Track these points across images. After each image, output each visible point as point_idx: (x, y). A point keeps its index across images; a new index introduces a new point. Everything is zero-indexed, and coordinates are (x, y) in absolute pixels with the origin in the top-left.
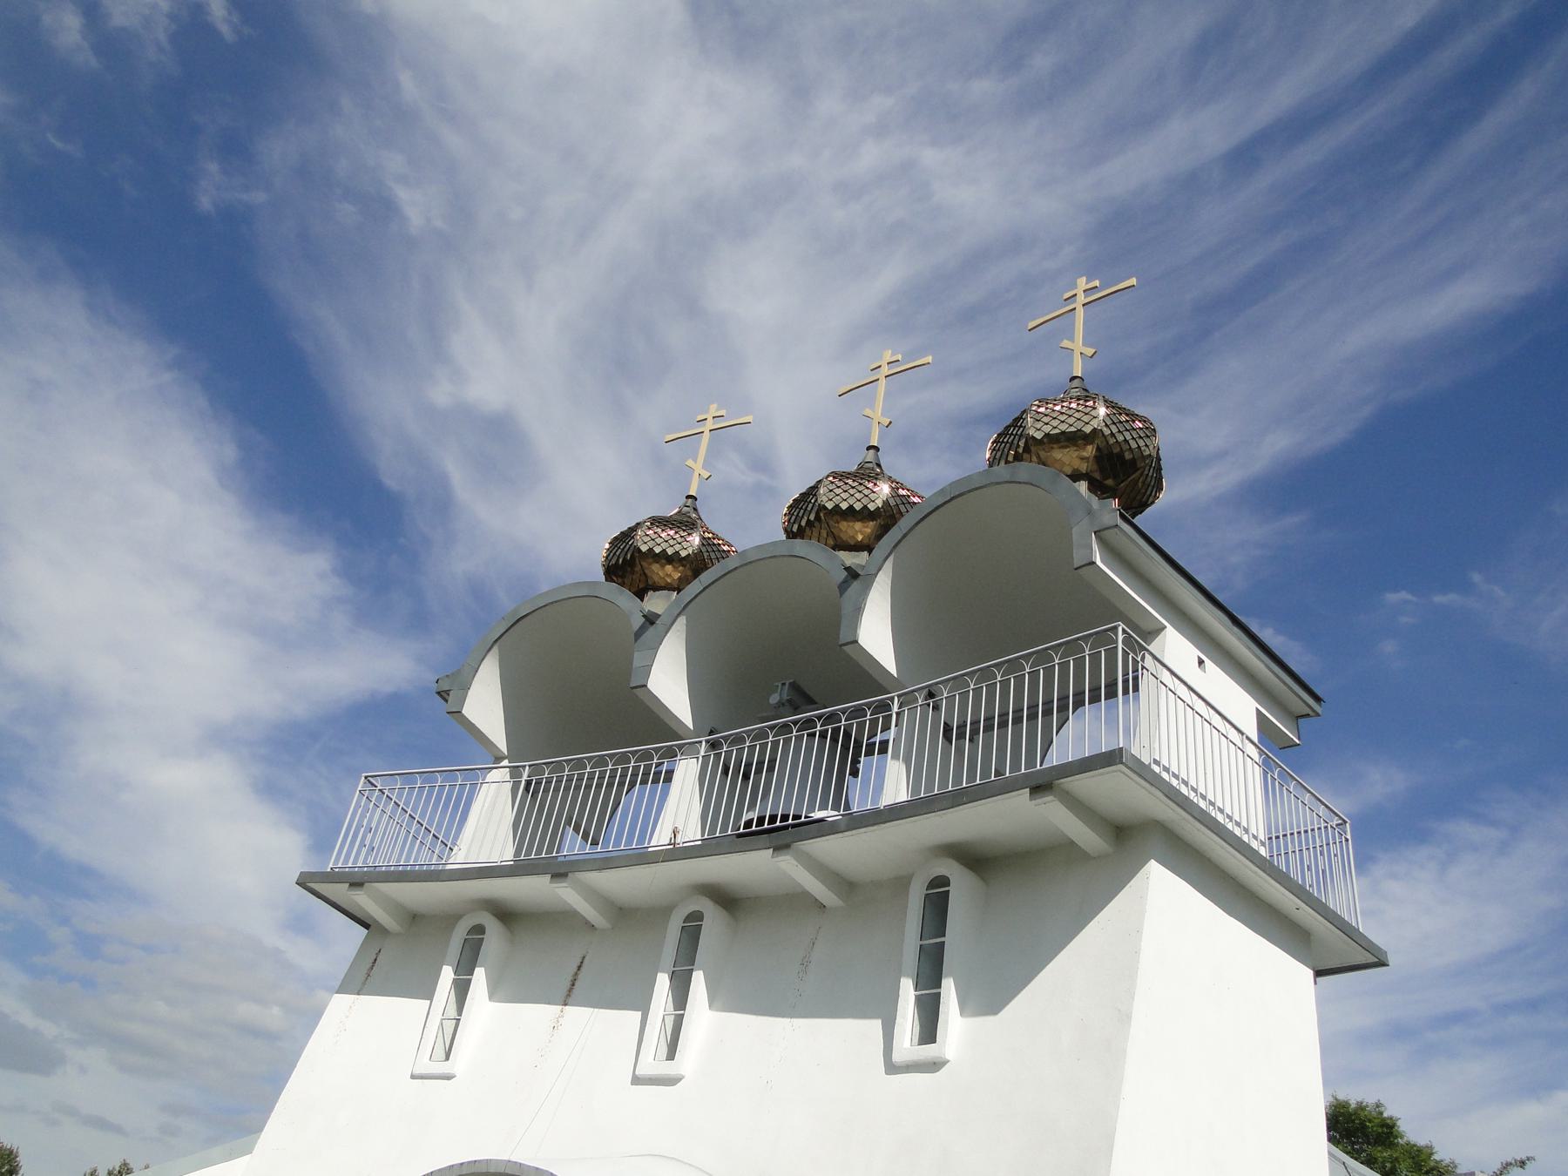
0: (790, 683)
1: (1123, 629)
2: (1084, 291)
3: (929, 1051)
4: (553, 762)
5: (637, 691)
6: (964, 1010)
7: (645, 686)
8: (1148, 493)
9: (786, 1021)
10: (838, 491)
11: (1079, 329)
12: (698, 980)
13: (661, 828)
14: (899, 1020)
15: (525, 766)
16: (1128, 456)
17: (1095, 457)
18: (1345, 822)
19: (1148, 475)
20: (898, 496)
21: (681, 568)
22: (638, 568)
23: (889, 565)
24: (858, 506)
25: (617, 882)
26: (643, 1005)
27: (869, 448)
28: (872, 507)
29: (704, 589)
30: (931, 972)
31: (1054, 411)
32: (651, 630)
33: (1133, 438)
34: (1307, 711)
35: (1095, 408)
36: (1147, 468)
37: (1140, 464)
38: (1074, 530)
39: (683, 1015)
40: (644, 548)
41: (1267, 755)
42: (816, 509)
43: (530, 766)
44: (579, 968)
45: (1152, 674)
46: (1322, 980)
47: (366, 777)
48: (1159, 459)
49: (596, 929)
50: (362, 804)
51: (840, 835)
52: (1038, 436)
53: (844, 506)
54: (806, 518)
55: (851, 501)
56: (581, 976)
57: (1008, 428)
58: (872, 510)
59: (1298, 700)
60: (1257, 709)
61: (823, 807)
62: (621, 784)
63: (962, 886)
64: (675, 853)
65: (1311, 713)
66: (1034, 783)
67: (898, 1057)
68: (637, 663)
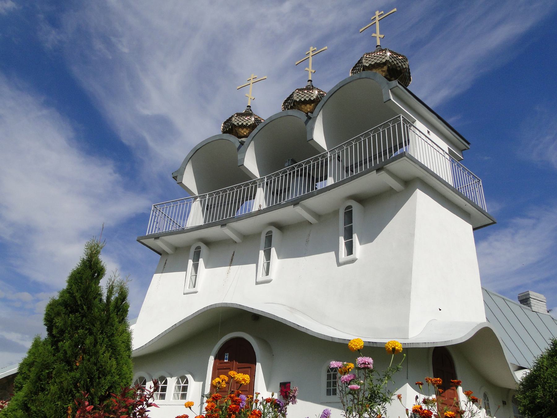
0: (291, 160)
1: (402, 116)
2: (378, 16)
3: (351, 257)
4: (216, 192)
5: (241, 167)
6: (361, 243)
7: (243, 165)
8: (406, 82)
9: (303, 258)
10: (300, 95)
11: (378, 33)
12: (273, 251)
13: (255, 207)
14: (340, 250)
15: (207, 194)
16: (399, 69)
17: (387, 70)
18: (480, 180)
19: (406, 75)
20: (321, 94)
21: (249, 129)
22: (234, 131)
23: (321, 113)
24: (307, 99)
25: (243, 225)
26: (256, 262)
27: (308, 81)
28: (312, 99)
29: (259, 131)
30: (349, 234)
31: (372, 56)
32: (242, 147)
33: (400, 62)
34: (465, 148)
35: (386, 53)
36: (405, 73)
37: (403, 71)
38: (383, 90)
39: (270, 262)
40: (236, 123)
41: (452, 158)
42: (293, 101)
43: (208, 194)
44: (233, 255)
45: (413, 131)
46: (476, 231)
47: (154, 206)
48: (409, 70)
49: (237, 243)
50: (154, 215)
51: (315, 197)
52: (367, 65)
53: (303, 100)
54: (290, 105)
55: (305, 97)
57: (357, 64)
58: (312, 100)
59: (462, 144)
60: (448, 147)
62: (239, 202)
64: (260, 212)
65: (467, 148)
66: (377, 168)
68: (239, 157)
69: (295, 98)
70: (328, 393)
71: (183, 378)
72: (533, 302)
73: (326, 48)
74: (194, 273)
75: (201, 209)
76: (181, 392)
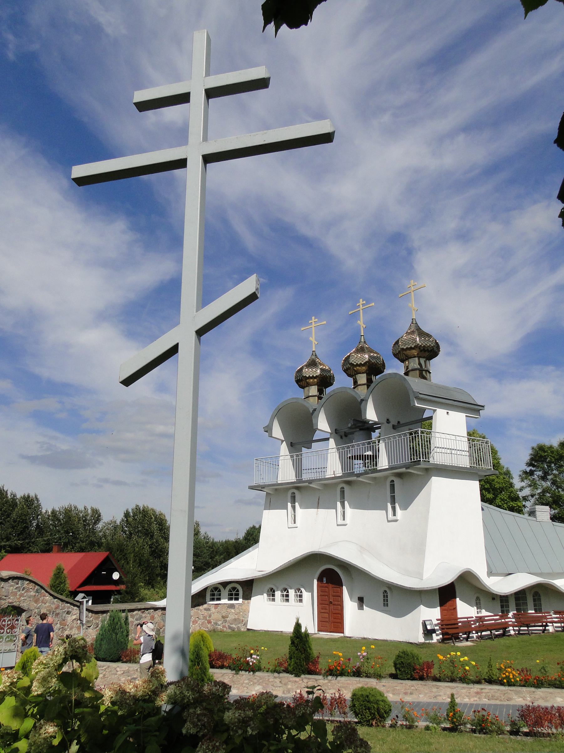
23: (371, 397)
30: (393, 502)
56: (319, 501)
61: (368, 451)
63: (397, 482)
67: (389, 519)
68: (314, 422)
69: (352, 360)
70: (384, 605)
71: (299, 590)
72: (538, 514)
73: (373, 304)
74: (293, 513)
75: (291, 463)
76: (298, 598)
